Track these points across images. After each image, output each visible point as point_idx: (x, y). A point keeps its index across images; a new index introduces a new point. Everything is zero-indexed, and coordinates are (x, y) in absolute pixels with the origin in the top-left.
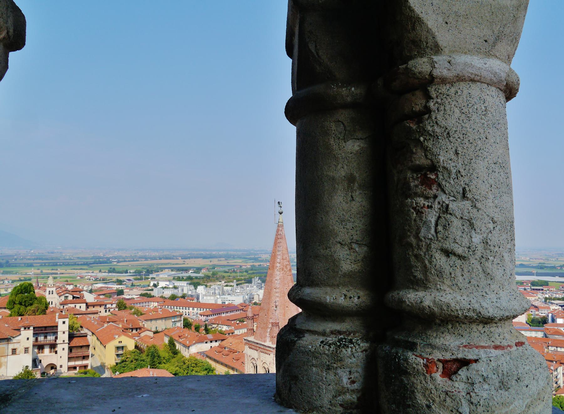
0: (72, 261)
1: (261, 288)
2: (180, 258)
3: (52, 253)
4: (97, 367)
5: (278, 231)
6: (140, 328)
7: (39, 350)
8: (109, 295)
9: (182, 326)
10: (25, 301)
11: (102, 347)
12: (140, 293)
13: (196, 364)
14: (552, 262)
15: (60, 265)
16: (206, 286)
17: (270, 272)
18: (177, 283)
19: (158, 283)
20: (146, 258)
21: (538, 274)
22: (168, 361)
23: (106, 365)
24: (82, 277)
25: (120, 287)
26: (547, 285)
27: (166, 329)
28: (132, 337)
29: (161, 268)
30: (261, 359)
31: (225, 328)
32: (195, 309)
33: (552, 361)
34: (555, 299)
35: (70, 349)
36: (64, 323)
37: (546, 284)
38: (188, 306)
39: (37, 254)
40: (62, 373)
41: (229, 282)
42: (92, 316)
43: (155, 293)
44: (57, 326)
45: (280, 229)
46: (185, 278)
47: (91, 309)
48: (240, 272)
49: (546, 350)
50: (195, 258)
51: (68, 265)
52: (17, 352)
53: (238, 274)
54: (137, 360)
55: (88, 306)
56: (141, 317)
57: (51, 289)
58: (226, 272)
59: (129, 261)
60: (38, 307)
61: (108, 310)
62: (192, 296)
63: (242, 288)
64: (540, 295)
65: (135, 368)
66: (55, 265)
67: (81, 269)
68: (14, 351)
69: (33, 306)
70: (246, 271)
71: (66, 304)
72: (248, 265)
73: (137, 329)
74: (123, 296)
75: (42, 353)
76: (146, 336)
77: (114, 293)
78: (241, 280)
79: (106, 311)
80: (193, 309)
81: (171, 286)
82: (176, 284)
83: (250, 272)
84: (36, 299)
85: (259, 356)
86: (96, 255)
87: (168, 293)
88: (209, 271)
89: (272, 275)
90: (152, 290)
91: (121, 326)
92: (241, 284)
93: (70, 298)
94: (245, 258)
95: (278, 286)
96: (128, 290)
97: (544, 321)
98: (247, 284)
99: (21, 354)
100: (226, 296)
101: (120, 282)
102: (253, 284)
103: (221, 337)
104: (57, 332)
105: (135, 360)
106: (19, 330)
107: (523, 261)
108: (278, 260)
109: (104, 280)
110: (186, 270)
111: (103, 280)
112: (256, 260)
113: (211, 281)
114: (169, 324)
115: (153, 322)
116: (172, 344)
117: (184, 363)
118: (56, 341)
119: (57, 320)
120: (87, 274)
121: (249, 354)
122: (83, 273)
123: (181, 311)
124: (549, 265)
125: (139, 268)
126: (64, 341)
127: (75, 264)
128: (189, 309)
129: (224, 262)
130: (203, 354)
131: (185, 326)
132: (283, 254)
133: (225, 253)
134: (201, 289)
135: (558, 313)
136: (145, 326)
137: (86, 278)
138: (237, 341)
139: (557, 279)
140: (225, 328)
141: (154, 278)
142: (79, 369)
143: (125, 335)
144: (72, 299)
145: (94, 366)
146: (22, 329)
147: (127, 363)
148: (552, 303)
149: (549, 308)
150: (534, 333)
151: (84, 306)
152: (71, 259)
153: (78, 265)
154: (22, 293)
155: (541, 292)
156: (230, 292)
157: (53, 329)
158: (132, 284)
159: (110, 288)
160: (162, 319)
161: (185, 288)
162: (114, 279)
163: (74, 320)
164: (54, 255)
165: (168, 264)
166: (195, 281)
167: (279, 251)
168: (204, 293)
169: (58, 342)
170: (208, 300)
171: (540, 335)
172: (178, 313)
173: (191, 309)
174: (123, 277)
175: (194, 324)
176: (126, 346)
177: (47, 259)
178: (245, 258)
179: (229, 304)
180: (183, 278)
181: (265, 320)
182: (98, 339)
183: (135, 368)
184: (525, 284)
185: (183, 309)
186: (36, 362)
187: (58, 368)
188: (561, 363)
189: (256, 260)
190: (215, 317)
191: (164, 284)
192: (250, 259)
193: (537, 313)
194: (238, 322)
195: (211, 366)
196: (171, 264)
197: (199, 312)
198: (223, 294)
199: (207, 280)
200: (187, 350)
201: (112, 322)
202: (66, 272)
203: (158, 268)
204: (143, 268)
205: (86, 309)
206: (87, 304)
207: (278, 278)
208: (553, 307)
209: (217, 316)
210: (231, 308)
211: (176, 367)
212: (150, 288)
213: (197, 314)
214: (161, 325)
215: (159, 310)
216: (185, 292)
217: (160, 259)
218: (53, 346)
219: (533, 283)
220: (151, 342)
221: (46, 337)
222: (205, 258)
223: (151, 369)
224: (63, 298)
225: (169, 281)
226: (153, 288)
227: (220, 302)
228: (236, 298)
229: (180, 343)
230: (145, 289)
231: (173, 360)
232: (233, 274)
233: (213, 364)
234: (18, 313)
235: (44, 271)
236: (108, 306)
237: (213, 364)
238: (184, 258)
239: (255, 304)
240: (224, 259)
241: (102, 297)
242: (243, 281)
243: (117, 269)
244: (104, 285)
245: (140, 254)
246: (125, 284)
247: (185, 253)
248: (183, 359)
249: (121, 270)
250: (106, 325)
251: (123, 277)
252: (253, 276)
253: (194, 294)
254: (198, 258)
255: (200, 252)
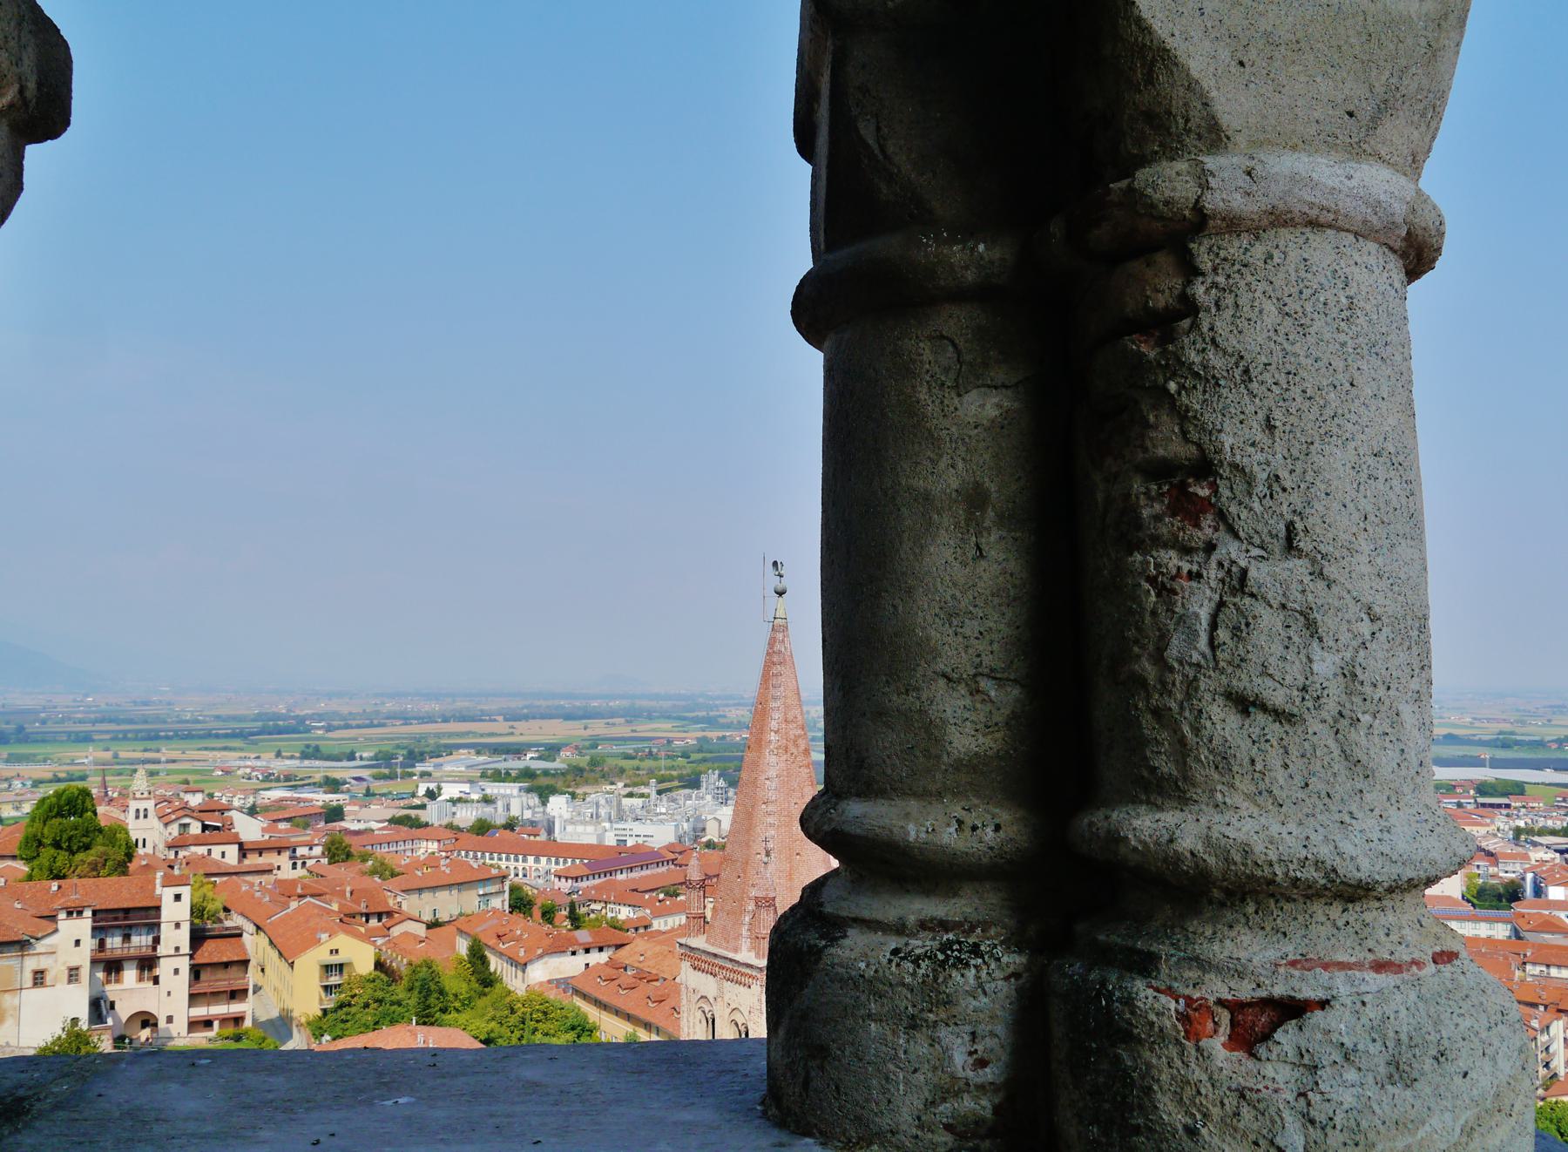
0: (199, 726)
1: (725, 802)
2: (500, 718)
3: (146, 704)
4: (271, 1022)
5: (772, 642)
6: (389, 914)
7: (109, 974)
8: (303, 821)
9: (506, 907)
10: (70, 839)
11: (284, 965)
12: (389, 814)
13: (545, 1013)
14: (1535, 730)
15: (168, 738)
16: (574, 796)
17: (749, 756)
18: (493, 789)
19: (439, 788)
20: (406, 719)
21: (1496, 764)
22: (467, 1003)
23: (295, 1014)
24: (227, 772)
25: (333, 799)
26: (1522, 793)
27: (461, 914)
28: (367, 938)
29: (446, 746)
30: (726, 999)
31: (625, 913)
32: (543, 860)
33: (1534, 1005)
34: (1543, 832)
35: (196, 972)
36: (178, 897)
37: (1518, 789)
38: (524, 851)
39: (103, 706)
40: (171, 1038)
41: (635, 785)
42: (256, 879)
43: (432, 814)
44: (158, 908)
45: (780, 636)
46: (513, 773)
47: (253, 860)
48: (669, 757)
49: (1518, 974)
50: (543, 717)
51: (190, 736)
52: (49, 978)
53: (663, 763)
54: (380, 1001)
55: (243, 851)
56: (392, 883)
57: (142, 805)
58: (627, 757)
59: (358, 727)
60: (105, 853)
61: (299, 863)
62: (533, 823)
63: (674, 800)
64: (1501, 821)
65: (377, 1023)
66: (153, 736)
67: (225, 749)
68: (39, 978)
69: (92, 851)
70: (685, 755)
71: (184, 846)
72: (691, 738)
73: (380, 916)
74: (343, 824)
75: (117, 981)
76: (406, 934)
77: (316, 816)
78: (671, 779)
79: (294, 866)
80: (537, 861)
81: (475, 797)
82: (488, 791)
83: (694, 756)
84: (100, 831)
85: (720, 989)
86: (267, 709)
87: (466, 816)
88: (581, 754)
89: (755, 764)
90: (423, 807)
91: (335, 907)
92: (669, 790)
93: (195, 828)
94: (682, 719)
95: (772, 796)
96: (356, 808)
97: (1512, 894)
98: (687, 791)
99: (58, 986)
100: (629, 825)
101: (333, 785)
102: (703, 789)
103: (615, 937)
104: (158, 925)
105: (376, 1001)
106: (52, 918)
107: (1454, 726)
108: (774, 725)
109: (289, 780)
110: (517, 751)
111: (288, 778)
112: (712, 722)
113: (587, 782)
114: (470, 901)
115: (426, 896)
116: (477, 956)
117: (513, 1011)
118: (154, 949)
119: (159, 890)
120: (242, 763)
121: (692, 985)
122: (231, 759)
123: (503, 864)
124: (1527, 738)
125: (387, 747)
126: (177, 949)
127: (209, 735)
128: (525, 861)
129: (623, 730)
130: (565, 984)
131: (513, 908)
132: (787, 707)
133: (625, 703)
134: (558, 805)
135: (1551, 870)
136: (405, 907)
137: (240, 772)
138: (658, 948)
139: (1549, 776)
140: (625, 913)
141: (429, 774)
142: (221, 1026)
143: (347, 932)
144: (199, 831)
145: (263, 1019)
146: (62, 915)
147: (353, 1010)
148: (1535, 844)
149: (1526, 857)
150: (1483, 925)
151: (232, 851)
152: (198, 722)
153: (217, 736)
154: (62, 816)
155: (1504, 812)
156: (639, 812)
157: (147, 917)
158: (368, 789)
159: (305, 800)
160: (449, 886)
161: (514, 801)
162: (318, 777)
163: (207, 889)
164: (149, 711)
165: (467, 734)
166: (544, 781)
167: (775, 698)
168: (567, 816)
169: (161, 950)
170: (579, 835)
171: (1501, 931)
172: (494, 872)
173: (531, 859)
174: (341, 771)
175: (539, 902)
176: (350, 964)
177: (131, 721)
178: (682, 719)
179: (637, 846)
180: (508, 774)
181: (737, 891)
182: (271, 943)
183: (377, 1023)
184: (1459, 790)
185: (508, 859)
186: (99, 1008)
187: (162, 1024)
188: (1559, 1011)
189: (712, 722)
190: (597, 881)
191: (455, 791)
192: (696, 720)
193: (1492, 870)
194: (661, 896)
195: (586, 1018)
196: (475, 734)
197: (554, 868)
198: (621, 819)
199: (575, 779)
200: (520, 973)
201: (312, 896)
202: (184, 757)
203: (439, 746)
204: (398, 747)
205: (240, 861)
206: (241, 845)
207: (772, 773)
208: (1537, 855)
209: (603, 879)
210: (642, 857)
211: (488, 1022)
212: (417, 802)
213: (548, 872)
214: (447, 904)
215: (443, 862)
216: (515, 812)
217: (446, 720)
218: (147, 964)
219: (1483, 789)
220: (420, 952)
221: (127, 938)
222: (569, 717)
223: (420, 1028)
224: (174, 830)
225: (471, 782)
226: (426, 800)
227: (610, 840)
228: (657, 830)
229: (501, 954)
230: (402, 803)
231: (481, 1003)
232: (649, 763)
233: (593, 1014)
234: (51, 871)
235: (123, 755)
236: (301, 851)
237: (593, 1014)
238: (513, 717)
239: (710, 845)
240: (622, 720)
241: (282, 826)
242: (676, 783)
243: (326, 748)
244: (288, 794)
245: (390, 706)
246: (348, 791)
247: (515, 704)
248: (508, 999)
249: (336, 751)
250: (294, 905)
251: (341, 771)
252: (702, 767)
253: (538, 817)
254: (551, 717)
255: (556, 702)
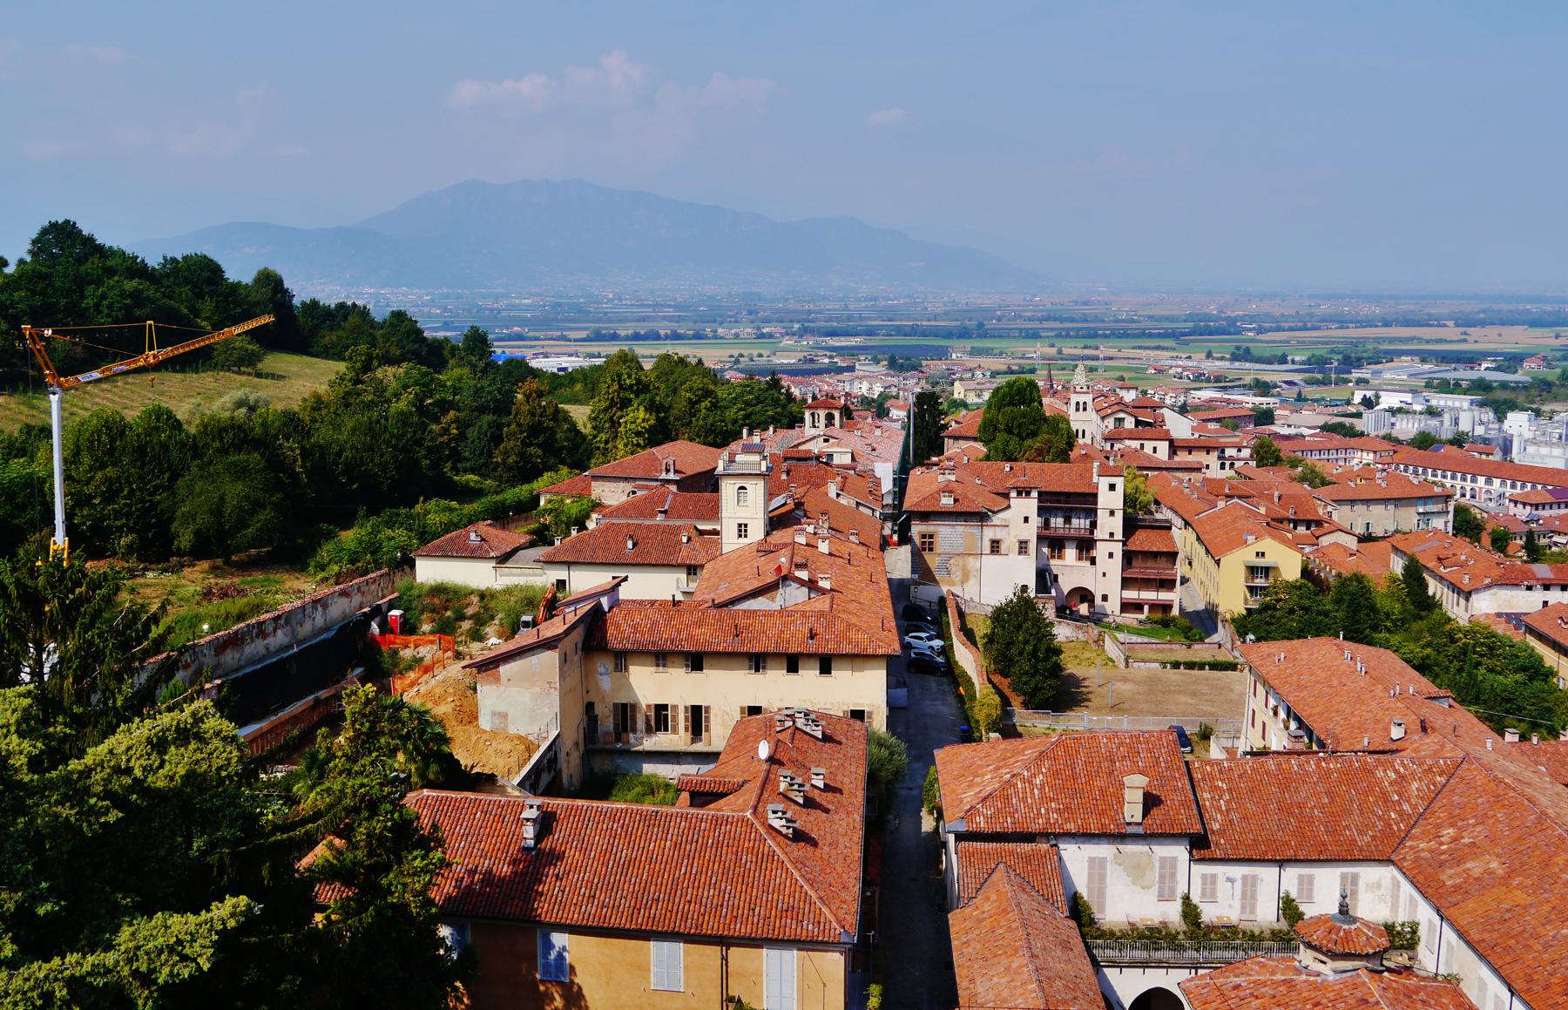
0: (1134, 325)
2: (1451, 323)
6: (1319, 523)
8: (1233, 423)
9: (1450, 529)
11: (1210, 562)
13: (1491, 648)
15: (1106, 336)
16: (1538, 413)
18: (1438, 400)
19: (1378, 397)
20: (1343, 323)
22: (1401, 624)
23: (1220, 610)
24: (1159, 371)
27: (1397, 531)
28: (1295, 544)
29: (1386, 352)
32: (1497, 482)
35: (1128, 557)
36: (1112, 487)
40: (1106, 615)
42: (1185, 476)
43: (1367, 423)
44: (1095, 496)
46: (1464, 384)
47: (1183, 457)
51: (1125, 335)
52: (1003, 548)
54: (1306, 609)
55: (1174, 448)
56: (1323, 492)
57: (1082, 399)
59: (1291, 329)
60: (1049, 441)
61: (1228, 463)
62: (1486, 441)
66: (1093, 335)
67: (1158, 348)
68: (995, 546)
71: (1120, 439)
73: (1308, 524)
74: (1273, 428)
75: (1060, 557)
76: (1336, 544)
77: (1246, 419)
79: (1223, 467)
80: (1489, 481)
81: (1418, 408)
82: (1434, 403)
84: (1045, 419)
87: (1406, 428)
88: (1550, 366)
90: (1359, 415)
91: (1262, 510)
93: (1129, 423)
96: (1287, 413)
101: (1263, 388)
104: (1095, 511)
106: (1006, 496)
109: (1219, 381)
110: (1471, 360)
113: (1556, 399)
114: (1408, 518)
115: (1359, 508)
116: (1414, 575)
117: (1453, 641)
118: (1092, 533)
119: (1095, 479)
122: (1164, 358)
123: (1448, 482)
125: (1321, 351)
126: (1112, 534)
128: (1473, 481)
130: (1516, 619)
131: (1458, 530)
134: (1517, 423)
136: (1335, 517)
137: (1172, 371)
141: (1366, 381)
143: (1273, 537)
146: (1013, 494)
151: (1163, 447)
152: (1133, 321)
153: (1151, 336)
157: (1086, 503)
158: (1300, 394)
160: (1385, 501)
161: (1465, 414)
162: (1248, 380)
164: (1089, 310)
166: (1501, 395)
168: (1528, 435)
169: (1098, 534)
170: (1543, 457)
172: (1437, 490)
173: (1481, 480)
175: (1489, 527)
176: (1276, 569)
177: (1073, 320)
180: (1457, 385)
182: (1198, 539)
185: (1453, 478)
186: (1045, 579)
187: (1098, 601)
191: (1395, 400)
195: (1541, 659)
196: (1420, 340)
197: (1508, 491)
200: (1462, 601)
201: (1240, 497)
203: (1377, 352)
204: (1332, 351)
206: (1171, 442)
212: (1352, 409)
213: (1502, 496)
214: (1382, 519)
216: (1465, 426)
217: (1387, 324)
218: (1086, 546)
220: (1349, 566)
221: (1068, 520)
222: (1535, 323)
223: (1347, 644)
224: (1110, 422)
225: (1414, 392)
226: (1362, 408)
229: (1441, 579)
230: (1336, 410)
231: (1416, 626)
235: (1065, 351)
236: (1229, 452)
238: (1466, 322)
241: (1212, 426)
243: (1257, 349)
244: (1218, 395)
245: (1325, 308)
246: (1279, 395)
247: (1469, 308)
249: (1267, 354)
250: (1221, 504)
254: (1514, 323)
255: (1521, 307)
